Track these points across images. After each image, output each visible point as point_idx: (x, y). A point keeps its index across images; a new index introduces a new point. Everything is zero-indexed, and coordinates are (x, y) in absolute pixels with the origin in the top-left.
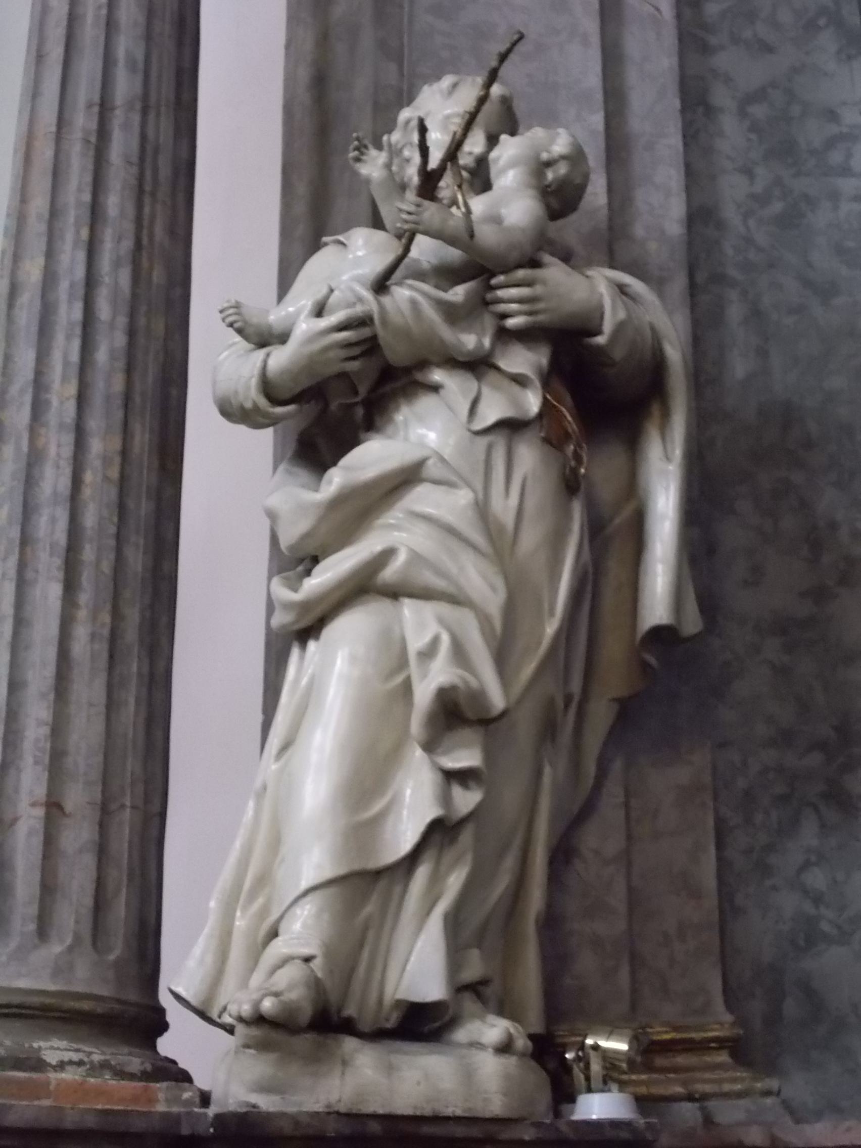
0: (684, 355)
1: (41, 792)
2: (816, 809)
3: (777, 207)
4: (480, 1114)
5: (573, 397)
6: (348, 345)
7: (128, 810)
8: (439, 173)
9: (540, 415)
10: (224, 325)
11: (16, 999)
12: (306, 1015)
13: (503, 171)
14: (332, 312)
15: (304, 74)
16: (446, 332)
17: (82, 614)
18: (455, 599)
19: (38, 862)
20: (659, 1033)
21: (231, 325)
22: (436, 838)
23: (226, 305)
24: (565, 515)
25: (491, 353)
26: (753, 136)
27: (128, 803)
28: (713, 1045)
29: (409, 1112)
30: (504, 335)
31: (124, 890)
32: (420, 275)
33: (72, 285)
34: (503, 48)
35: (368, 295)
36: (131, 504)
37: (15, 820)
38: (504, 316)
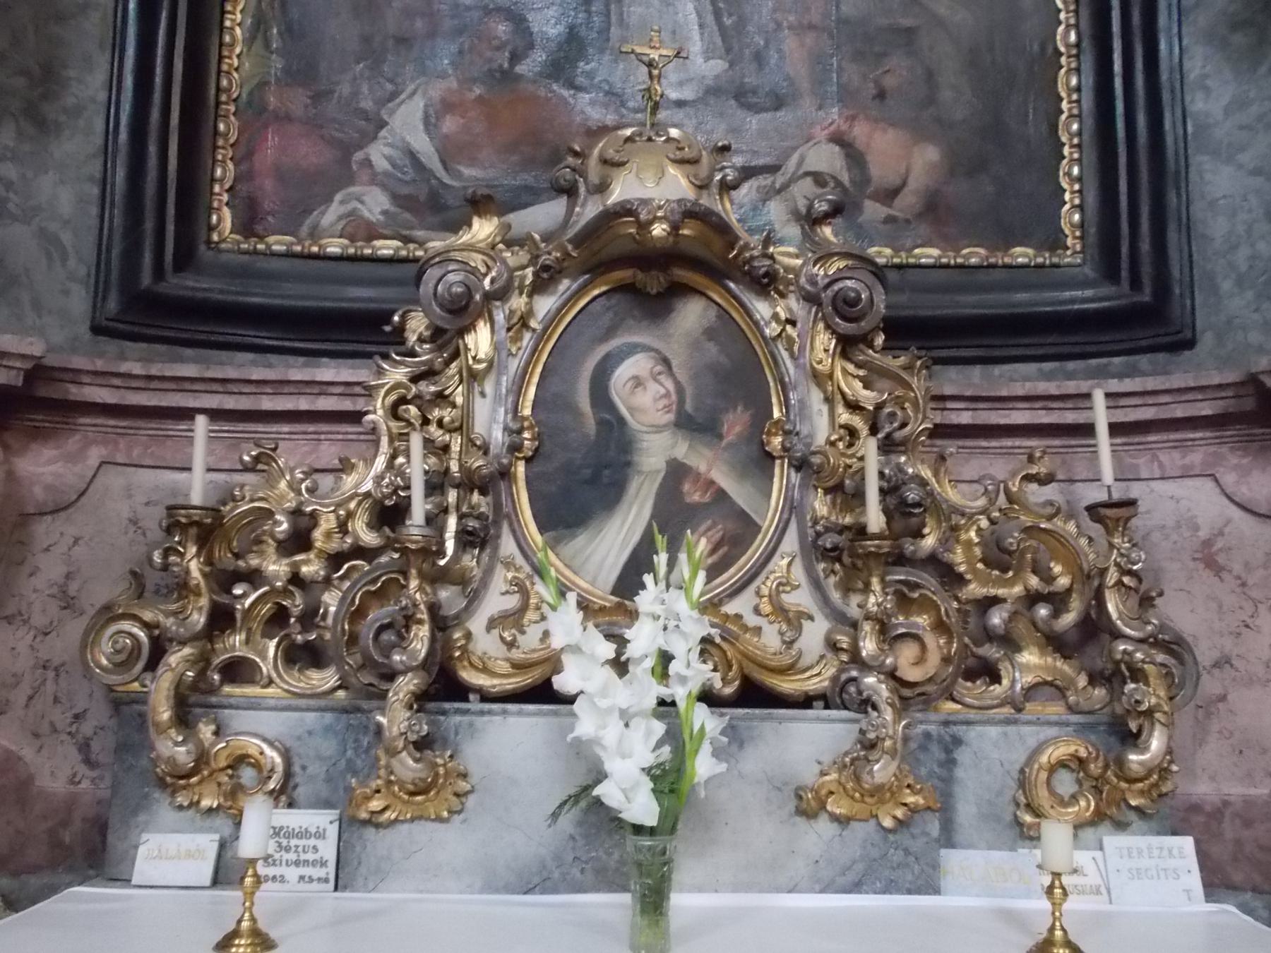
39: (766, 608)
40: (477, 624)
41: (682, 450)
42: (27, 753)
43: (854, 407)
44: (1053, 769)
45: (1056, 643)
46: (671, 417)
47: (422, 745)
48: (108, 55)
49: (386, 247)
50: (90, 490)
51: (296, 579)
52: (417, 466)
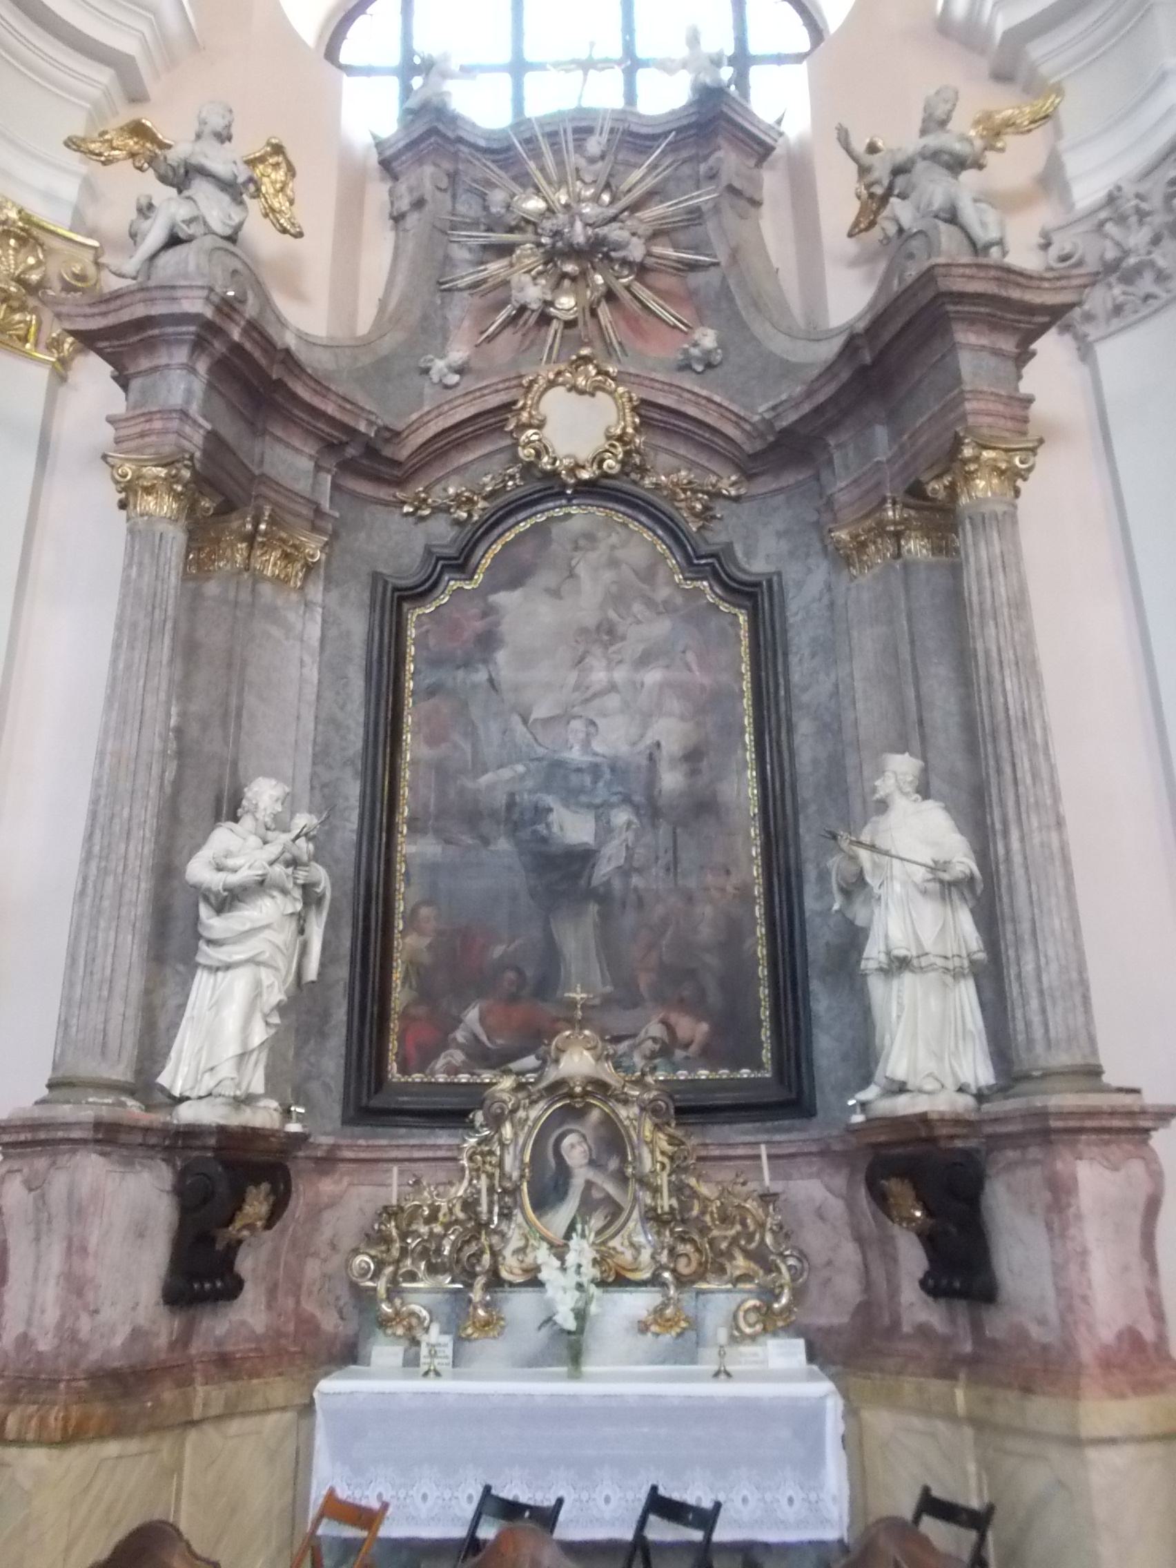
39: (626, 1243)
40: (508, 1252)
41: (591, 1174)
42: (318, 1314)
43: (663, 1153)
44: (747, 1312)
45: (748, 1255)
46: (586, 1161)
47: (487, 1306)
49: (464, 1078)
51: (431, 1233)
52: (483, 1183)
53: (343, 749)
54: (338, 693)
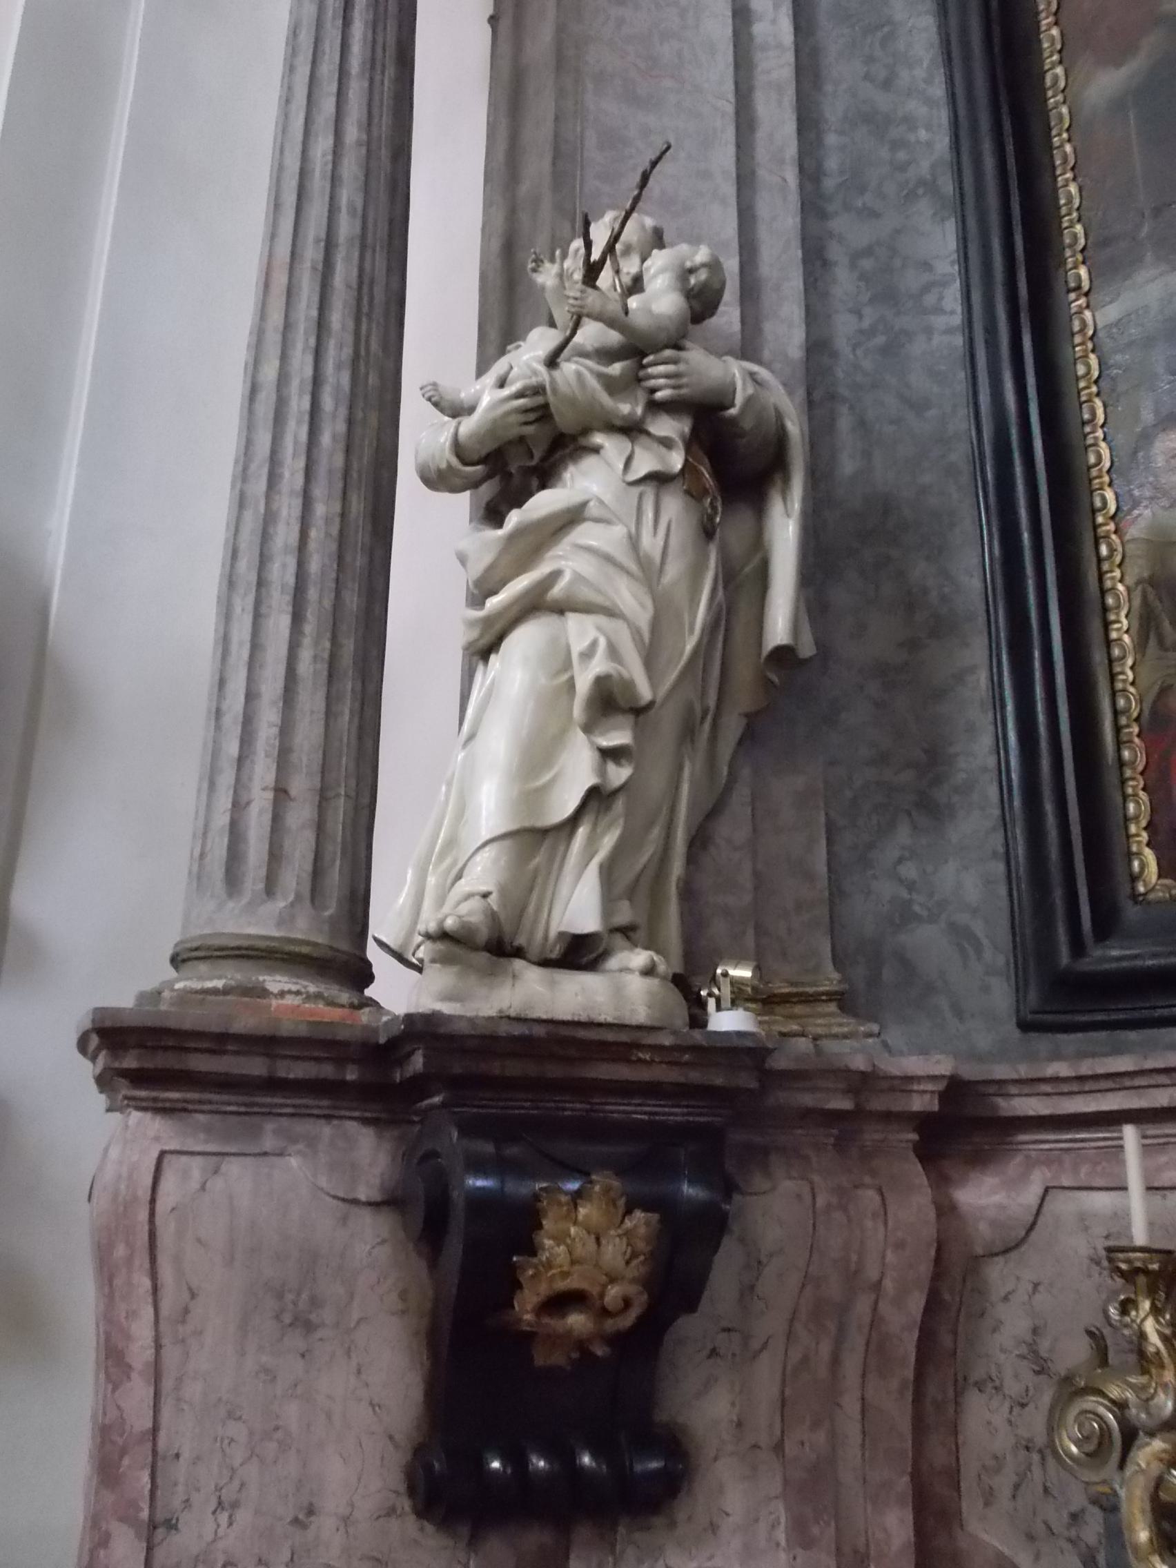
0: (801, 430)
1: (270, 778)
2: (910, 814)
3: (880, 340)
4: (627, 1022)
5: (711, 461)
6: (526, 411)
7: (342, 800)
8: (600, 264)
9: (683, 470)
10: (420, 393)
11: (245, 943)
12: (483, 935)
13: (655, 276)
14: (512, 383)
15: (496, 244)
16: (605, 399)
17: (307, 641)
18: (611, 612)
19: (267, 835)
20: (780, 987)
21: (429, 399)
22: (593, 804)
23: (425, 383)
24: (706, 557)
25: (642, 420)
26: (862, 284)
27: (343, 793)
28: (824, 998)
29: (568, 1017)
30: (655, 407)
31: (338, 863)
32: (584, 354)
33: (302, 381)
34: (653, 157)
35: (542, 369)
36: (348, 558)
37: (248, 803)
38: (653, 391)
48: (990, 715)
50: (1039, 1222)
53: (902, 168)
54: (870, 60)
